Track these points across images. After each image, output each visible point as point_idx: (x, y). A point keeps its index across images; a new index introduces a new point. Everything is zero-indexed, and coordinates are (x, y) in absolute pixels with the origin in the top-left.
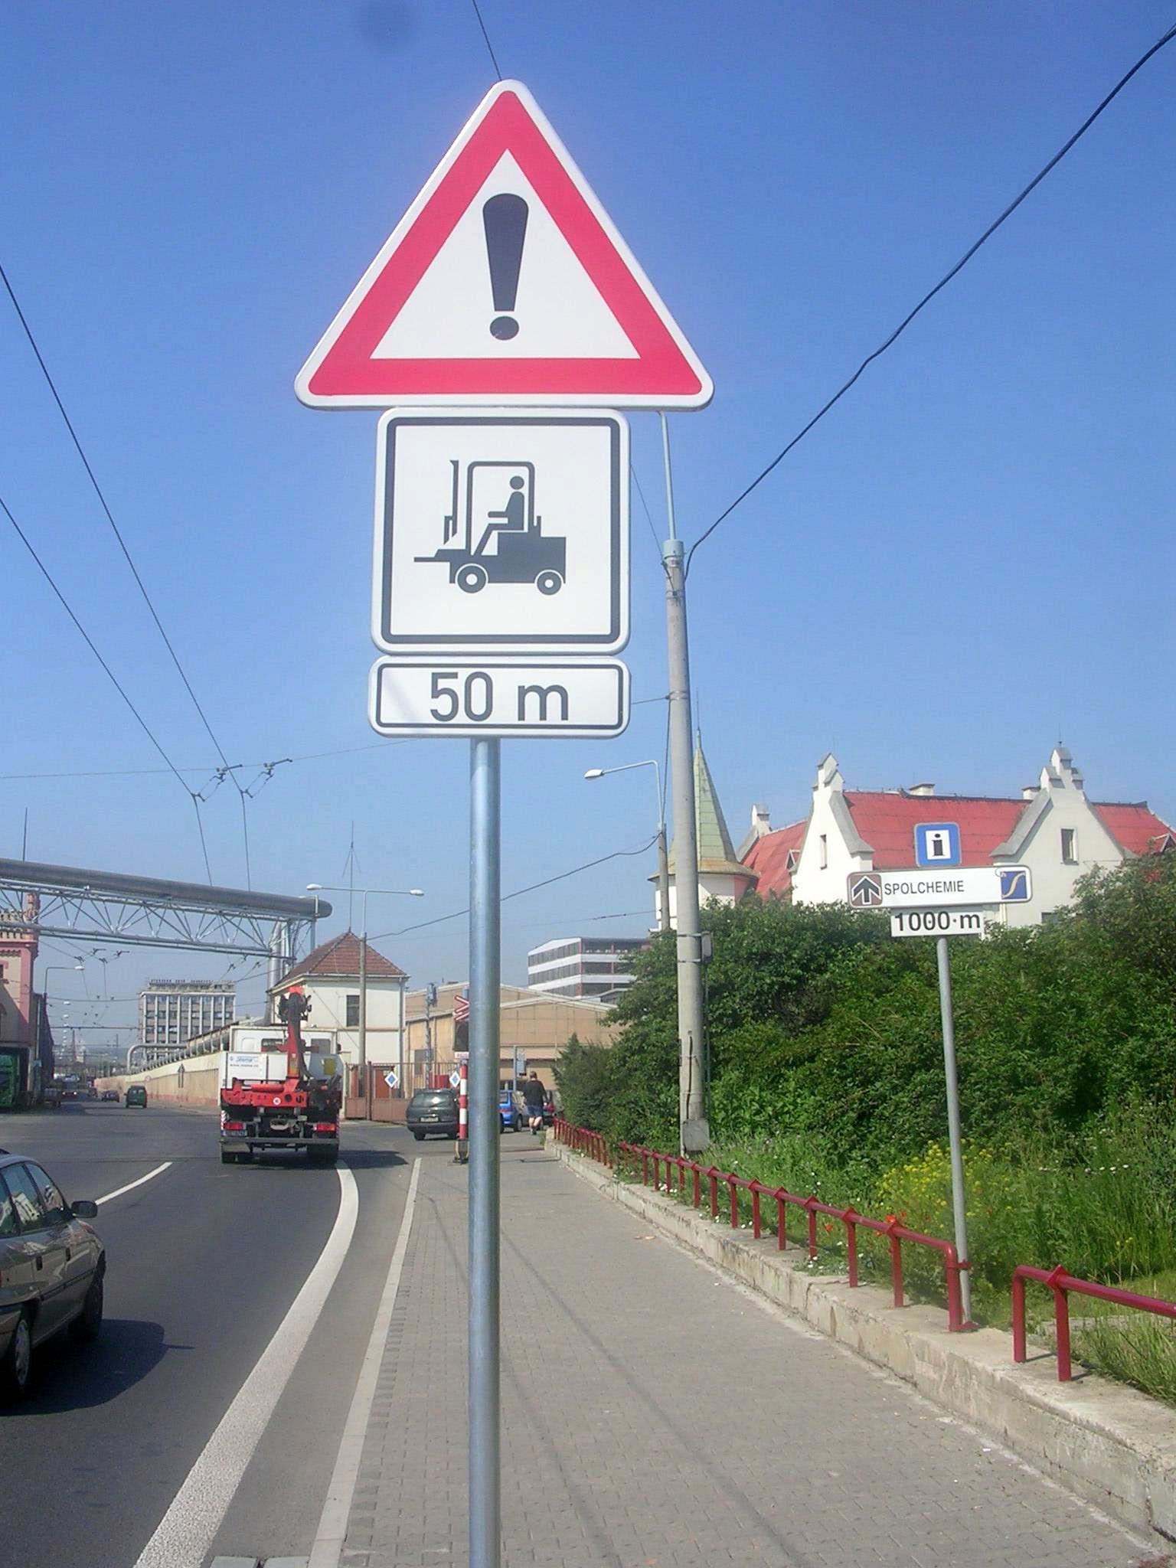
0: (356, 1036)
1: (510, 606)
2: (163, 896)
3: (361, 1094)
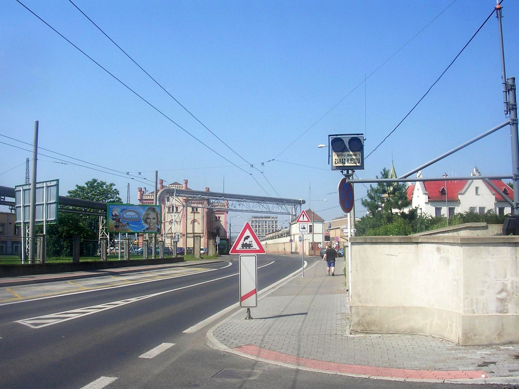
0: (312, 235)
1: (304, 230)
2: (263, 201)
3: (313, 249)
